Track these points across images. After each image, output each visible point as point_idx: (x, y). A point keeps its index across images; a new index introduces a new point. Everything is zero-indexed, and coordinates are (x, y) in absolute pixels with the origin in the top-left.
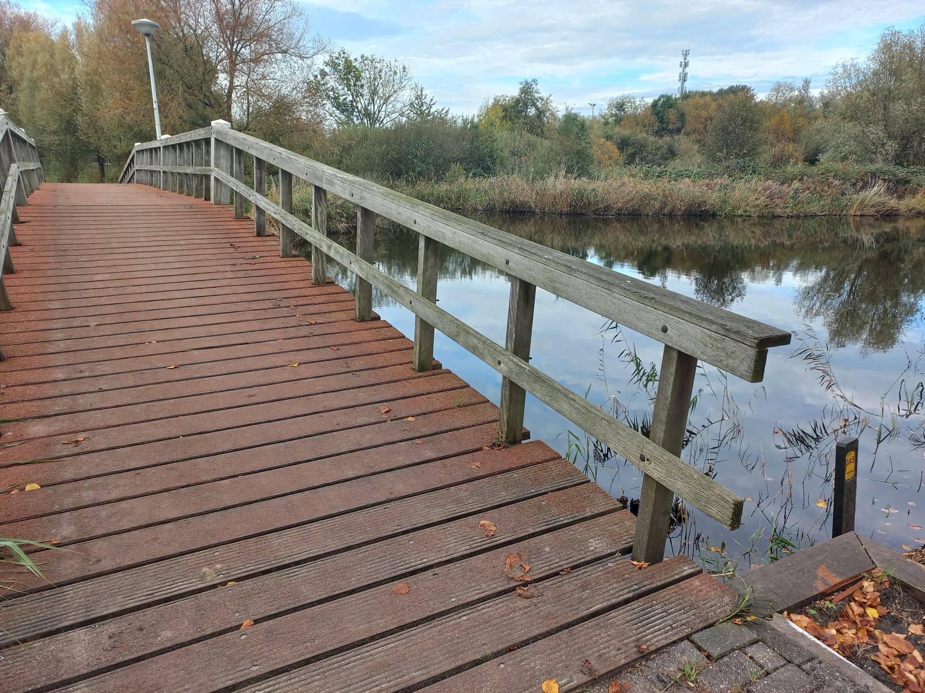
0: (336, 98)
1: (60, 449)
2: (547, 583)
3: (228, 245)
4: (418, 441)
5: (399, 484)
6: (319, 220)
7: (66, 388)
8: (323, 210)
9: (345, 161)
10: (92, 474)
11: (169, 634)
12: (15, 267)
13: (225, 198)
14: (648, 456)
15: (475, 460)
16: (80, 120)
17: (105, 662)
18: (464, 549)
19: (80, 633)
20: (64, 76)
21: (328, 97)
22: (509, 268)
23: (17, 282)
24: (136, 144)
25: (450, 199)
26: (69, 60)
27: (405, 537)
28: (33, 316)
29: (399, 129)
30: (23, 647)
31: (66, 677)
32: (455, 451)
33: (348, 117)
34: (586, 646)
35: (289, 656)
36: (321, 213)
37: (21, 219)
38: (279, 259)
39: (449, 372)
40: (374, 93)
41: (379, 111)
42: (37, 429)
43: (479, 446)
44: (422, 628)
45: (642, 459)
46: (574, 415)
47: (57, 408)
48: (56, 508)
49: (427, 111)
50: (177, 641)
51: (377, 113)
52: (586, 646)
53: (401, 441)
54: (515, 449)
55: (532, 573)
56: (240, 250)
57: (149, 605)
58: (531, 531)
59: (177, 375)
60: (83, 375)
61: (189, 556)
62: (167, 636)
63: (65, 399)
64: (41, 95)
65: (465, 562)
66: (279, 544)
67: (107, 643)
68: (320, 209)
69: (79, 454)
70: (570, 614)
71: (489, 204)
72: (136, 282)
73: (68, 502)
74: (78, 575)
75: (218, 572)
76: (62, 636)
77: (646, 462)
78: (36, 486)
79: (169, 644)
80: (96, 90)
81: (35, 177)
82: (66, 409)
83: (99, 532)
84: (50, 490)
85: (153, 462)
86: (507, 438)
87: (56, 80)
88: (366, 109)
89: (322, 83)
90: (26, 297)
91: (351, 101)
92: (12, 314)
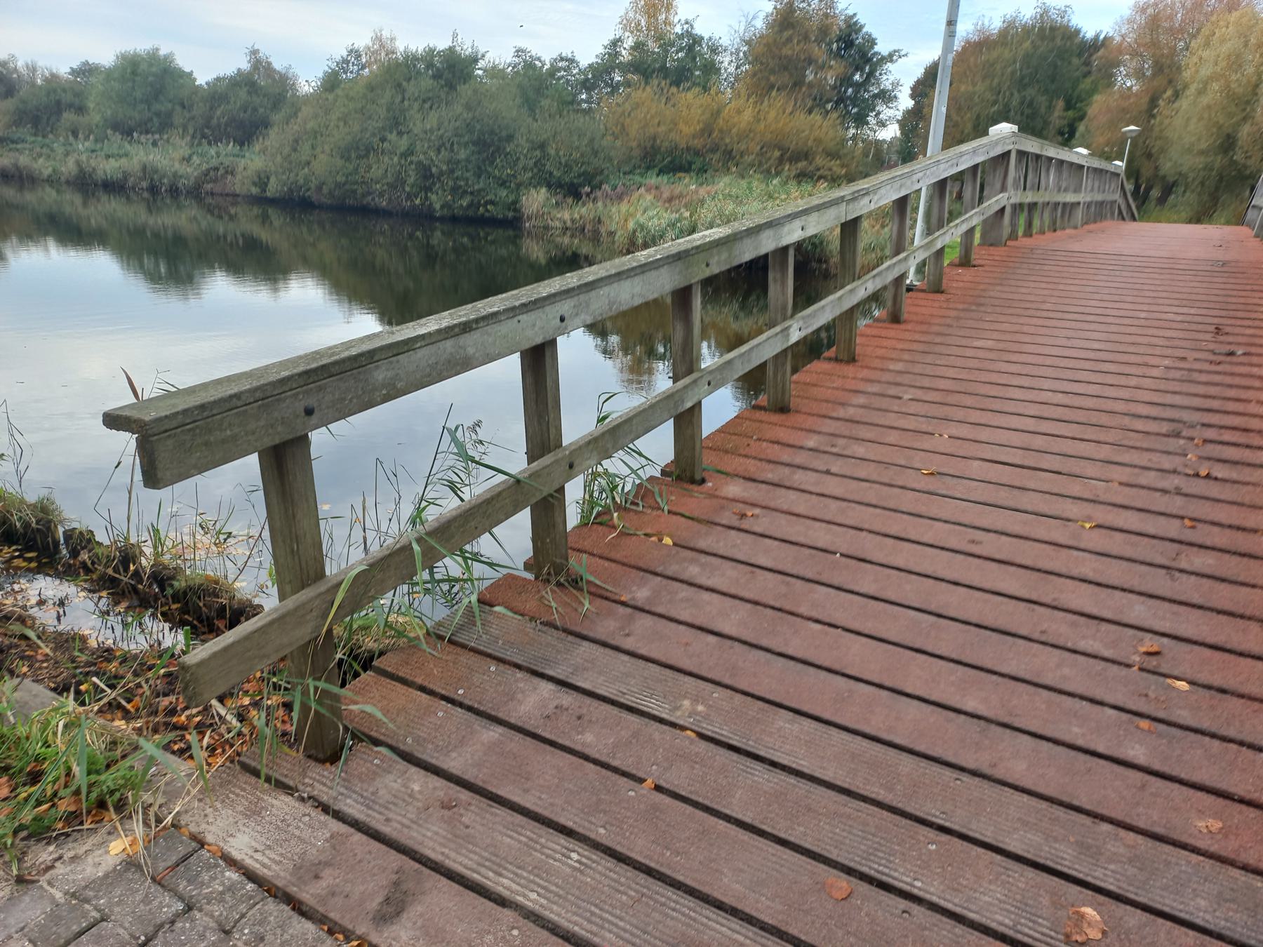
3: (1212, 328)
12: (905, 316)
28: (865, 373)
32: (1196, 777)
64: (1205, 100)
81: (1079, 214)
92: (849, 370)
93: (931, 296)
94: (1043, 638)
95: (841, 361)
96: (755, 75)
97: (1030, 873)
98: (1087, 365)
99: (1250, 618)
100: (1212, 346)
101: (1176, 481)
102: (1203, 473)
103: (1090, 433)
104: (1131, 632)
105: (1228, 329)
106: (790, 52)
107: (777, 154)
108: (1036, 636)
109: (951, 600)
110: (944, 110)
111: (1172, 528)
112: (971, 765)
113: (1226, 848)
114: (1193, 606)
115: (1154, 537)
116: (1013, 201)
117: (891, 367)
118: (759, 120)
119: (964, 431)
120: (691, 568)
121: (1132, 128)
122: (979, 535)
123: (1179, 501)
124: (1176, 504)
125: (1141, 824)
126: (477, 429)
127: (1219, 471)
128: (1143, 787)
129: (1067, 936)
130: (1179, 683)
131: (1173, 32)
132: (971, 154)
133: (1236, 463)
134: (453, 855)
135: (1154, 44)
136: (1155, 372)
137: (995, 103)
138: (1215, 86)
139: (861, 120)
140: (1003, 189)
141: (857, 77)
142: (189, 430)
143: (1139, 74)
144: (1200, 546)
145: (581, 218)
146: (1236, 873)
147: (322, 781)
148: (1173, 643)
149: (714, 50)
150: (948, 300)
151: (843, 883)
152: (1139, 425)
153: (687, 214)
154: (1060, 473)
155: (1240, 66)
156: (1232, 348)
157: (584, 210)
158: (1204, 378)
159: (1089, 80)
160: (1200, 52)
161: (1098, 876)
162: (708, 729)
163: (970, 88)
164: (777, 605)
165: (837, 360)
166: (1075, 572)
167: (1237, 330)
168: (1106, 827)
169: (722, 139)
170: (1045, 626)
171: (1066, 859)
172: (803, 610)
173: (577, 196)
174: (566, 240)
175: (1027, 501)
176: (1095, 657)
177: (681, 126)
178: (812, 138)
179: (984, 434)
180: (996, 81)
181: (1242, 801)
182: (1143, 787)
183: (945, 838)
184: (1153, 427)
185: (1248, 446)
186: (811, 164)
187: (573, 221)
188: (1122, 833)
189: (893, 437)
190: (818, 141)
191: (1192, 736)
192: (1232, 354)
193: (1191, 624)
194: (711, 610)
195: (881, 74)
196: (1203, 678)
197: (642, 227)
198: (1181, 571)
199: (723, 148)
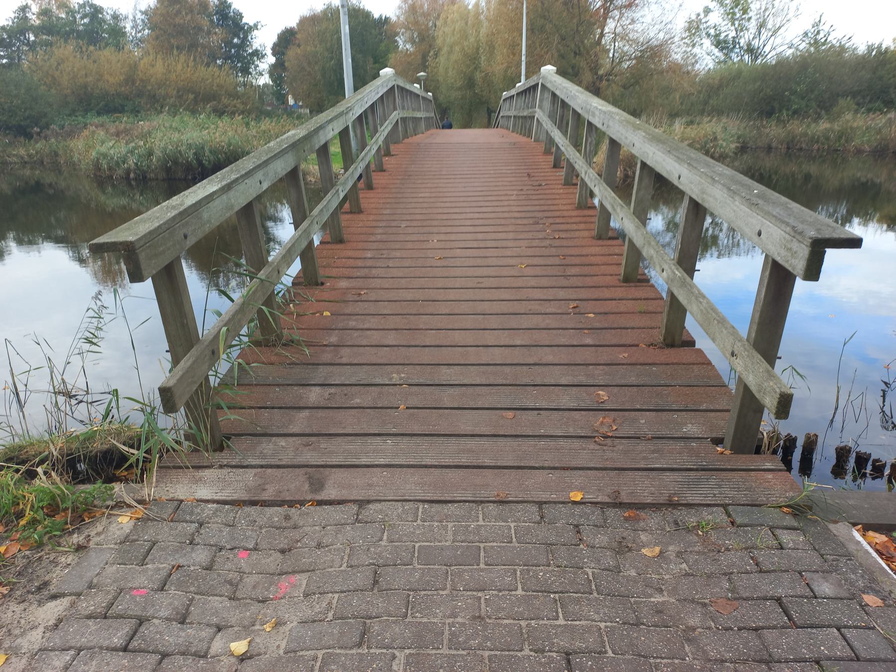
0: (717, 35)
1: (350, 297)
2: (623, 441)
3: (526, 175)
4: (586, 331)
5: (548, 356)
6: (588, 149)
7: (369, 263)
8: (592, 141)
9: (711, 102)
10: (360, 313)
11: (358, 401)
12: (374, 186)
13: (543, 137)
14: (736, 352)
15: (625, 352)
16: (478, 76)
17: (322, 404)
18: (572, 405)
19: (317, 389)
20: (472, 39)
21: (708, 35)
22: (679, 182)
23: (372, 195)
24: (504, 93)
25: (827, 139)
26: (478, 24)
27: (532, 388)
28: (372, 217)
29: (782, 63)
30: (289, 388)
31: (302, 405)
32: (612, 343)
33: (726, 55)
34: (625, 484)
35: (416, 429)
36: (590, 144)
37: (392, 153)
38: (560, 186)
39: (653, 286)
40: (762, 25)
41: (764, 46)
42: (343, 284)
43: (636, 343)
44: (509, 439)
45: (733, 354)
46: (699, 316)
47: (358, 274)
48: (334, 327)
49: (823, 40)
50: (361, 405)
51: (762, 47)
52: (625, 484)
53: (572, 329)
54: (667, 351)
55: (616, 432)
56: (533, 179)
57: (356, 385)
58: (638, 407)
59: (439, 263)
60: (382, 256)
61: (389, 366)
62: (357, 401)
63: (365, 270)
64: (454, 57)
65: (567, 413)
66: (445, 373)
67: (326, 396)
68: (590, 140)
69: (358, 301)
70: (628, 463)
71: (880, 144)
72: (445, 200)
73: (340, 325)
74: (329, 362)
75: (401, 379)
76: (308, 388)
77: (735, 357)
78: (328, 314)
79: (356, 406)
80: (492, 47)
81: (423, 124)
82: (363, 275)
83: (349, 344)
84: (334, 317)
85: (397, 312)
86: (664, 340)
87: (465, 44)
88: (749, 44)
89: (703, 21)
90: (373, 206)
91: (734, 38)
92: (361, 216)
93: (380, 173)
94: (531, 312)
95: (355, 213)
96: (157, 38)
97: (574, 389)
98: (481, 199)
99: (602, 287)
100: (530, 183)
101: (548, 242)
102: (557, 237)
103: (500, 229)
104: (563, 302)
105: (533, 174)
106: (182, 21)
107: (191, 96)
108: (528, 312)
109: (486, 307)
110: (350, 60)
111: (557, 261)
112: (532, 362)
113: (633, 360)
114: (580, 287)
115: (551, 266)
116: (401, 116)
117: (384, 212)
118: (170, 72)
119: (443, 237)
120: (351, 323)
121: (422, 74)
122: (480, 280)
123: (553, 250)
124: (553, 251)
125: (602, 362)
126: (99, 297)
127: (563, 235)
128: (596, 351)
129: (597, 402)
130: (590, 315)
131: (426, 15)
132: (373, 91)
133: (567, 231)
134: (329, 460)
135: (416, 23)
136: (513, 198)
137: (332, 58)
138: (457, 48)
139: (246, 71)
140: (395, 109)
141: (235, 40)
142: (149, 247)
143: (412, 41)
144: (571, 265)
145: (37, 153)
146: (639, 367)
147: (224, 457)
148: (580, 302)
149: (116, 17)
150: (390, 175)
151: (510, 414)
152: (519, 222)
153: (142, 143)
154: (497, 248)
155: (467, 37)
156: (540, 182)
157: (38, 146)
158: (535, 197)
159: (383, 45)
160: (442, 28)
161: (596, 382)
162: (410, 381)
163: (313, 49)
164: (407, 328)
165: (351, 212)
166: (529, 285)
167: (537, 174)
168: (591, 367)
169: (145, 87)
170: (529, 307)
171: (583, 379)
172: (421, 327)
173: (29, 136)
174: (28, 172)
175: (490, 261)
176: (555, 314)
177: (106, 77)
178: (215, 85)
179: (453, 237)
180: (329, 44)
181: (630, 346)
182: (596, 351)
183: (537, 388)
184: (525, 221)
185: (568, 223)
186: (219, 103)
187: (30, 156)
188: (598, 367)
189: (409, 245)
190: (220, 86)
191: (604, 331)
192: (540, 185)
193: (584, 294)
194: (376, 337)
195: (252, 39)
196: (597, 311)
197: (105, 156)
198: (569, 276)
199: (147, 93)
